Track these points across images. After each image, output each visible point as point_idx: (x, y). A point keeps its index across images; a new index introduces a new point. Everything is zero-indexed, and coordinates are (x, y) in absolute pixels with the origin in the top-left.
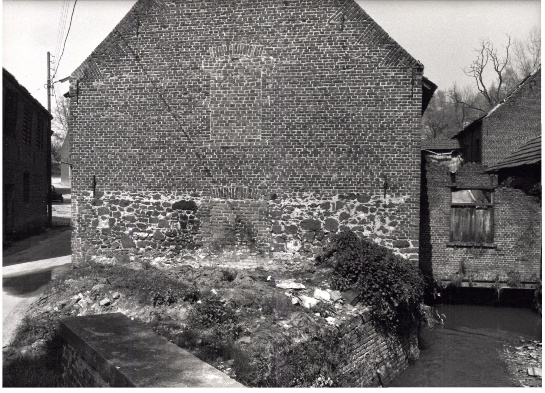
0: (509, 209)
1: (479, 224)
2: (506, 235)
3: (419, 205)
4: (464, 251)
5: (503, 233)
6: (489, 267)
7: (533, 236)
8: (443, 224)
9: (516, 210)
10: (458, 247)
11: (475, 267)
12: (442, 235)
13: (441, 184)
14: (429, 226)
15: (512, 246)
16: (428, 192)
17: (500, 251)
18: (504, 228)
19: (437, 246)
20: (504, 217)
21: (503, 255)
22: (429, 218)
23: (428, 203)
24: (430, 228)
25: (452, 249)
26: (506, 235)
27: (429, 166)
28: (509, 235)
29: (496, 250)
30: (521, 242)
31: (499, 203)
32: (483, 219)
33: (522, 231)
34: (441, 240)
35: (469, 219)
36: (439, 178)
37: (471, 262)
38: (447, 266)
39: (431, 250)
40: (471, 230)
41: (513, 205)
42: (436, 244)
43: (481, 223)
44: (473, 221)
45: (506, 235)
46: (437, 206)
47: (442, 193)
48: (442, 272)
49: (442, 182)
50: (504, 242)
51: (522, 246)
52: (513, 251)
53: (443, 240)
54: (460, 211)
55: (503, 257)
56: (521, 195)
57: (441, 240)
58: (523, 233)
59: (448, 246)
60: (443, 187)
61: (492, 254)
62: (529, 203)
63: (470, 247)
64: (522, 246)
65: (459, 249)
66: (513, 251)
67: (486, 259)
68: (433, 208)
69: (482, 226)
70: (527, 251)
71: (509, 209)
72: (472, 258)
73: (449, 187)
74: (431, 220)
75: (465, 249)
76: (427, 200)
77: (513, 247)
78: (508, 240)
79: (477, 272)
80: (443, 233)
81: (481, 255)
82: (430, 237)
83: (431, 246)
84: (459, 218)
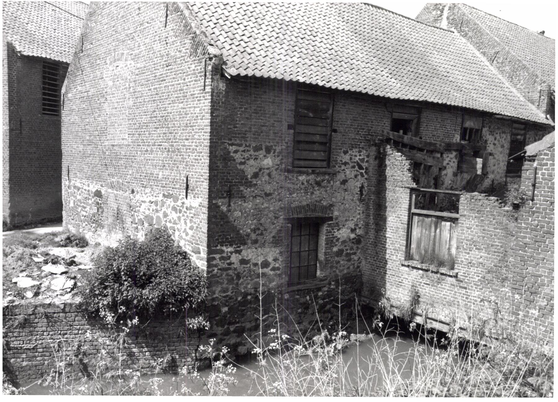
0: (477, 226)
1: (444, 243)
2: (470, 264)
3: (207, 209)
4: (420, 274)
5: (467, 259)
6: (447, 302)
7: (506, 271)
8: (399, 237)
9: (486, 228)
10: (414, 268)
11: (431, 297)
12: (397, 250)
13: (400, 184)
14: (385, 237)
15: (477, 278)
16: (387, 192)
17: (462, 282)
18: (469, 253)
19: (392, 263)
20: (470, 237)
21: (465, 288)
22: (385, 226)
23: (386, 207)
24: (386, 239)
25: (406, 269)
26: (470, 263)
27: (389, 160)
28: (474, 264)
29: (457, 280)
30: (489, 277)
31: (464, 216)
32: (449, 235)
33: (492, 261)
34: (397, 256)
35: (433, 234)
36: (399, 176)
37: (426, 291)
38: (401, 289)
39: (386, 266)
40: (434, 250)
41: (482, 221)
42: (391, 260)
43: (446, 242)
44: (438, 237)
45: (470, 263)
46: (395, 212)
47: (401, 195)
48: (395, 296)
49: (401, 181)
50: (467, 271)
51: (490, 282)
52: (478, 285)
53: (399, 257)
54: (423, 221)
55: (464, 291)
56: (495, 206)
57: (397, 256)
58: (493, 264)
59: (403, 265)
60: (402, 187)
61: (451, 285)
62: (505, 220)
63: (427, 271)
64: (490, 282)
65: (415, 270)
66: (478, 285)
67: (444, 289)
68: (390, 214)
69: (447, 246)
70: (496, 290)
71: (477, 226)
72: (429, 284)
73: (408, 188)
74: (388, 230)
75: (421, 272)
76: (385, 203)
77: (479, 280)
78: (473, 270)
79: (432, 306)
80: (399, 248)
81: (439, 283)
82: (386, 250)
83: (386, 261)
84: (422, 231)
